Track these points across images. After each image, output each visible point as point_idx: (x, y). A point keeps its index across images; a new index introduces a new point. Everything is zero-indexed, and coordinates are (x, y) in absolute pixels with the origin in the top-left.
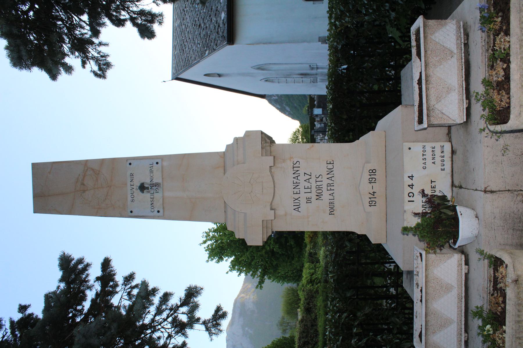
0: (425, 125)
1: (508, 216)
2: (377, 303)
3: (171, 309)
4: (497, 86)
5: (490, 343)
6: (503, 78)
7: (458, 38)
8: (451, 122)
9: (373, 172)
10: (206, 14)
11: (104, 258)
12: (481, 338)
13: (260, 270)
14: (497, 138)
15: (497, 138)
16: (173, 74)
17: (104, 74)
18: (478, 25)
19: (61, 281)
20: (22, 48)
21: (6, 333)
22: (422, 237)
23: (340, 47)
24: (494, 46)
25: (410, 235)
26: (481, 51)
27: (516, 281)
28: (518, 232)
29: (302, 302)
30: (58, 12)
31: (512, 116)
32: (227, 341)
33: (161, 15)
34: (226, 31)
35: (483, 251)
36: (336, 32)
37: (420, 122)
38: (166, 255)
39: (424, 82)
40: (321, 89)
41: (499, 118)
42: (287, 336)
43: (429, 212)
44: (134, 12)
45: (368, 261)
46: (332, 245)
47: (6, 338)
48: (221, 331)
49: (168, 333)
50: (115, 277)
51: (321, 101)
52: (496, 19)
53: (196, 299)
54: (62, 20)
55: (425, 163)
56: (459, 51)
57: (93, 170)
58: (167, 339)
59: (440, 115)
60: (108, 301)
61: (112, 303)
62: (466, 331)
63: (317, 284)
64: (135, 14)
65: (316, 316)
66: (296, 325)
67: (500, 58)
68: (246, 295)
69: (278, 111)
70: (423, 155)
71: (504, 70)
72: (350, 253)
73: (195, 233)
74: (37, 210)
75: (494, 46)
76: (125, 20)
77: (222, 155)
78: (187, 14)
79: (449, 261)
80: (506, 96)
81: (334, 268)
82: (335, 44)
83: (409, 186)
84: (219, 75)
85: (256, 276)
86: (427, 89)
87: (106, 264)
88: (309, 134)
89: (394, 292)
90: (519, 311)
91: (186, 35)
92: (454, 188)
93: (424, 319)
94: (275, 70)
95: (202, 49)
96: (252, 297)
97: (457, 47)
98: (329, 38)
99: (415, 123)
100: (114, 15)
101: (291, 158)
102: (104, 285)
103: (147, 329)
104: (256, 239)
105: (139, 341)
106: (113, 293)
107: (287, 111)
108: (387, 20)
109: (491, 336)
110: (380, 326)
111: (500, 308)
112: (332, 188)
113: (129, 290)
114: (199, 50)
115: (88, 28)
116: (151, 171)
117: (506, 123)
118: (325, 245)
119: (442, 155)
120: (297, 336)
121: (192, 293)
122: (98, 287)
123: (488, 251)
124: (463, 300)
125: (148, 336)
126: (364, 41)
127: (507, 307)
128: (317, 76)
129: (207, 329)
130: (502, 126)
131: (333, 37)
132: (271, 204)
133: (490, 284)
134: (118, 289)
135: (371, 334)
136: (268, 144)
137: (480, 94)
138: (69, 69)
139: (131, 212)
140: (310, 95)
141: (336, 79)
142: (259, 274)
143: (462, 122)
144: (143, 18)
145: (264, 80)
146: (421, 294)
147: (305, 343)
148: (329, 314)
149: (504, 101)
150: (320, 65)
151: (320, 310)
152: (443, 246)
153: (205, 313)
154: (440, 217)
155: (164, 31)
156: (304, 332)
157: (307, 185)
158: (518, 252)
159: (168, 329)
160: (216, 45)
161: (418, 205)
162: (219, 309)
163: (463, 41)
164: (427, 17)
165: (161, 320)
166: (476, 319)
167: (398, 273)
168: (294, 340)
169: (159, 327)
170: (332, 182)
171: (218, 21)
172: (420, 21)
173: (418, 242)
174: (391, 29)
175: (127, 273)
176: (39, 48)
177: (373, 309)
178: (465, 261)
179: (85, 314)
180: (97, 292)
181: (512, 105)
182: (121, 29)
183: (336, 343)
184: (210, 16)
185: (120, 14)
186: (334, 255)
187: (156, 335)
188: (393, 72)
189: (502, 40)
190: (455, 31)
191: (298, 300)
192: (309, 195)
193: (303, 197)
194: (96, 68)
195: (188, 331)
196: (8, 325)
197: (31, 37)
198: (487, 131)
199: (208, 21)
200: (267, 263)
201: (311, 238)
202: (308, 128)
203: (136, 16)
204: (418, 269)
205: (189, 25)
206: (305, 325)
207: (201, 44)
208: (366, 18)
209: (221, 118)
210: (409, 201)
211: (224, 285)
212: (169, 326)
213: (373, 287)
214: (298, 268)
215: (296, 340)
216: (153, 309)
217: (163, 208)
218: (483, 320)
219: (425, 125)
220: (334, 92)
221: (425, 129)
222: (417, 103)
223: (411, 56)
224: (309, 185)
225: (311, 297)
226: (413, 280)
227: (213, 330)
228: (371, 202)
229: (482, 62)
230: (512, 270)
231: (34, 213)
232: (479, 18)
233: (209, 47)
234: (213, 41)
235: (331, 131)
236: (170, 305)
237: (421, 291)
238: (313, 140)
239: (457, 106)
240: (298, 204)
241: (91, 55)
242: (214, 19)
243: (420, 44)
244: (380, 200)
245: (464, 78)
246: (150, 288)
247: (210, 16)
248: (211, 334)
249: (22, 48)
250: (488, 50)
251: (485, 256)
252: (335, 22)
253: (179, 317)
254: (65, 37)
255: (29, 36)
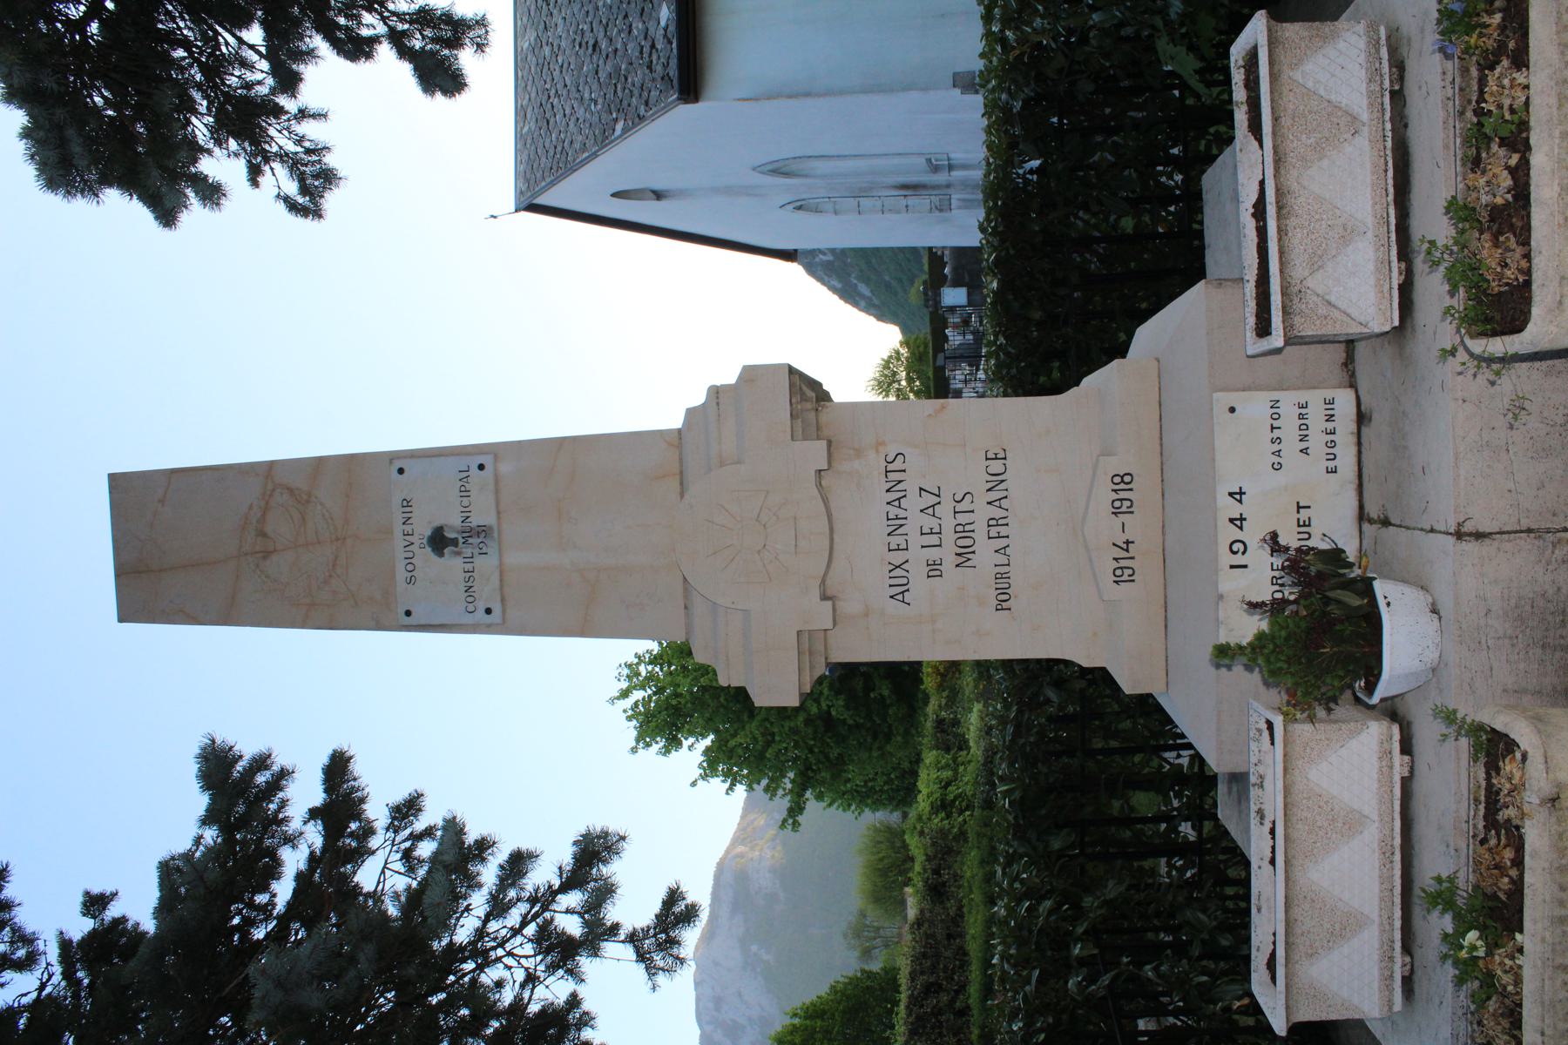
0: (1276, 339)
1: (1528, 608)
2: (1141, 867)
3: (533, 900)
4: (1492, 220)
5: (1476, 984)
6: (1509, 197)
7: (1374, 74)
8: (1354, 330)
9: (1123, 481)
10: (615, 10)
11: (1210, 649)
12: (1450, 971)
13: (791, 775)
14: (1492, 378)
15: (1492, 378)
16: (519, 194)
17: (316, 204)
18: (1432, 37)
19: (206, 821)
20: (71, 132)
21: (50, 976)
22: (1273, 673)
23: (1018, 105)
24: (1481, 99)
25: (1238, 669)
26: (1442, 114)
27: (1554, 800)
28: (1558, 654)
29: (917, 868)
30: (173, 20)
31: (1536, 311)
32: (697, 984)
33: (482, 23)
34: (674, 63)
35: (1455, 711)
36: (1007, 62)
37: (1263, 329)
38: (513, 741)
39: (1271, 210)
40: (963, 228)
41: (1498, 317)
42: (876, 967)
43: (1292, 598)
44: (400, 16)
45: (1114, 744)
46: (1005, 700)
47: (48, 989)
48: (682, 961)
49: (527, 969)
50: (365, 807)
51: (965, 265)
52: (1486, 19)
53: (605, 870)
54: (186, 44)
55: (1278, 453)
56: (1376, 115)
57: (291, 490)
58: (523, 986)
59: (1322, 310)
60: (346, 879)
61: (357, 884)
62: (1407, 949)
63: (961, 812)
64: (402, 21)
65: (960, 908)
66: (900, 935)
67: (1499, 135)
68: (752, 849)
69: (836, 297)
70: (1273, 428)
71: (1513, 171)
72: (1061, 720)
73: (593, 673)
74: (127, 613)
75: (1481, 99)
76: (374, 40)
77: (674, 440)
78: (555, 12)
79: (1354, 744)
80: (1519, 251)
81: (1011, 765)
82: (1004, 96)
83: (1231, 520)
84: (658, 195)
85: (780, 792)
86: (1281, 231)
87: (337, 768)
88: (930, 370)
89: (1192, 836)
90: (1562, 889)
91: (556, 74)
92: (1366, 526)
93: (1281, 915)
94: (823, 176)
95: (604, 116)
96: (769, 854)
97: (1371, 105)
98: (985, 76)
99: (1249, 334)
100: (339, 27)
101: (880, 444)
102: (333, 831)
103: (464, 961)
104: (778, 685)
105: (442, 996)
106: (360, 854)
107: (862, 296)
108: (1159, 23)
109: (1481, 963)
110: (1150, 935)
111: (1506, 880)
112: (1004, 531)
113: (408, 844)
114: (595, 119)
115: (264, 65)
116: (464, 492)
117: (1520, 330)
118: (985, 696)
119: (1330, 426)
120: (904, 966)
121: (594, 851)
122: (314, 836)
123: (1470, 711)
124: (1398, 857)
125: (466, 979)
126: (1090, 87)
127: (1528, 878)
128: (949, 191)
129: (642, 957)
130: (1507, 339)
131: (996, 77)
132: (823, 582)
133: (1476, 810)
134: (374, 843)
135: (1125, 960)
136: (809, 405)
137: (1439, 244)
138: (212, 193)
139: (408, 613)
140: (930, 249)
141: (1007, 202)
142: (789, 786)
143: (1387, 328)
144: (428, 33)
145: (791, 207)
146: (1271, 843)
147: (931, 989)
148: (1000, 903)
149: (1514, 266)
150: (958, 156)
151: (971, 891)
152: (1335, 700)
153: (634, 907)
154: (1325, 614)
155: (491, 71)
156: (924, 955)
157: (929, 522)
158: (1557, 714)
159: (527, 957)
160: (647, 103)
161: (1260, 577)
162: (673, 896)
163: (1387, 84)
164: (1279, 14)
165: (504, 932)
166: (1436, 913)
167: (1200, 781)
168: (895, 980)
169: (500, 952)
170: (1003, 513)
171: (651, 32)
172: (1257, 28)
173: (1262, 688)
174: (1171, 49)
175: (399, 796)
176: (120, 131)
177: (1131, 887)
178: (1401, 742)
179: (279, 917)
180: (312, 853)
181: (1537, 277)
182: (363, 67)
183: (1022, 988)
184: (626, 16)
185: (360, 24)
186: (1010, 729)
187: (489, 976)
188: (1179, 178)
189: (1506, 82)
190: (1363, 55)
191: (904, 861)
192: (934, 554)
193: (917, 558)
194: (291, 188)
195: (585, 963)
196: (52, 953)
197: (97, 99)
198: (1462, 356)
199: (620, 32)
200: (811, 751)
201: (942, 675)
202: (926, 346)
203: (406, 26)
204: (1261, 769)
205: (563, 44)
206: (928, 936)
207: (600, 101)
208: (1096, 17)
209: (665, 326)
210: (1232, 567)
211: (686, 823)
212: (529, 949)
213: (1129, 820)
214: (906, 765)
215: (903, 979)
216: (479, 901)
217: (503, 600)
218: (1458, 917)
219: (1276, 339)
220: (1002, 241)
221: (1278, 351)
222: (1251, 275)
223: (1232, 127)
224: (934, 523)
225: (944, 851)
226: (1248, 799)
227: (658, 959)
228: (1118, 572)
229: (1446, 147)
230: (1542, 767)
231: (121, 620)
232: (1436, 15)
233: (624, 109)
234: (636, 92)
235: (997, 359)
236: (530, 888)
237: (1272, 832)
238: (940, 388)
239: (1372, 281)
240: (905, 581)
241: (275, 149)
242: (638, 26)
243: (1258, 97)
244: (1146, 565)
245: (1391, 198)
246: (471, 838)
247: (626, 16)
248: (652, 970)
249: (71, 132)
250: (1462, 113)
251: (1461, 728)
252: (1002, 31)
253: (556, 923)
254: (197, 96)
255: (91, 97)
